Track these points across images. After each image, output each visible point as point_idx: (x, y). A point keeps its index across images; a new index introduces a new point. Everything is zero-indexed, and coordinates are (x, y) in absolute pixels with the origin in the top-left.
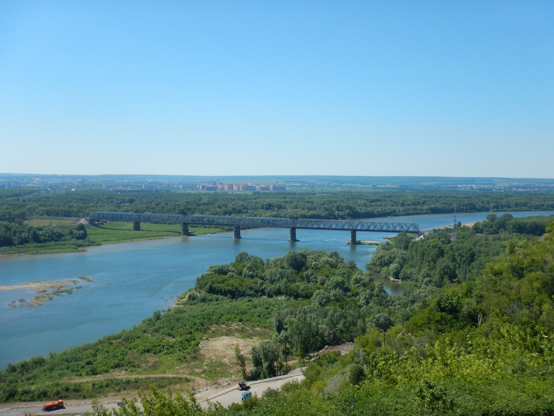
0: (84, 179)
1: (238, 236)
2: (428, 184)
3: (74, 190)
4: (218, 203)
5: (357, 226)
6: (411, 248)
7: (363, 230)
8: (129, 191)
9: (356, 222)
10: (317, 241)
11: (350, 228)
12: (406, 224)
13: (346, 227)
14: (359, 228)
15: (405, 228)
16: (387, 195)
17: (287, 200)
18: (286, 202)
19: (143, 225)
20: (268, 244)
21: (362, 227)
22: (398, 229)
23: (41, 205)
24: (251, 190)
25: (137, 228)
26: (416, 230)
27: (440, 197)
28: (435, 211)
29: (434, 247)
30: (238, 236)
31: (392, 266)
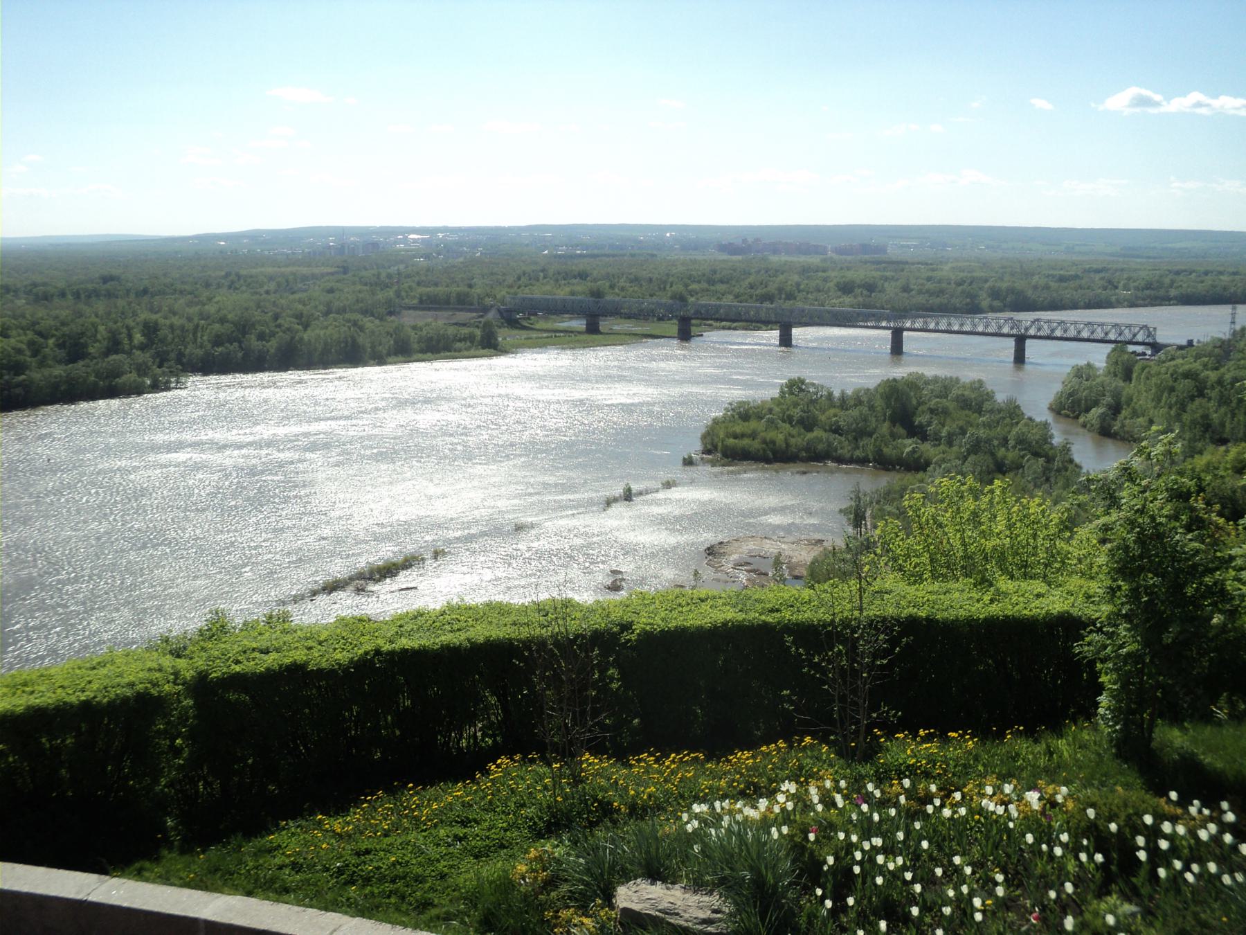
0: (495, 234)
1: (786, 341)
2: (1182, 245)
3: (1040, 103)
4: (751, 279)
5: (1027, 329)
6: (1139, 378)
7: (1041, 338)
8: (581, 256)
9: (1026, 317)
10: (945, 355)
11: (1015, 331)
12: (1129, 326)
13: (1005, 330)
14: (1032, 332)
15: (1127, 335)
16: (1095, 266)
17: (888, 274)
18: (886, 279)
19: (604, 325)
20: (845, 360)
21: (1039, 329)
22: (1112, 336)
23: (419, 284)
24: (817, 253)
25: (593, 329)
26: (1150, 340)
27: (1206, 273)
28: (1189, 300)
29: (1187, 375)
30: (786, 341)
31: (1096, 412)
